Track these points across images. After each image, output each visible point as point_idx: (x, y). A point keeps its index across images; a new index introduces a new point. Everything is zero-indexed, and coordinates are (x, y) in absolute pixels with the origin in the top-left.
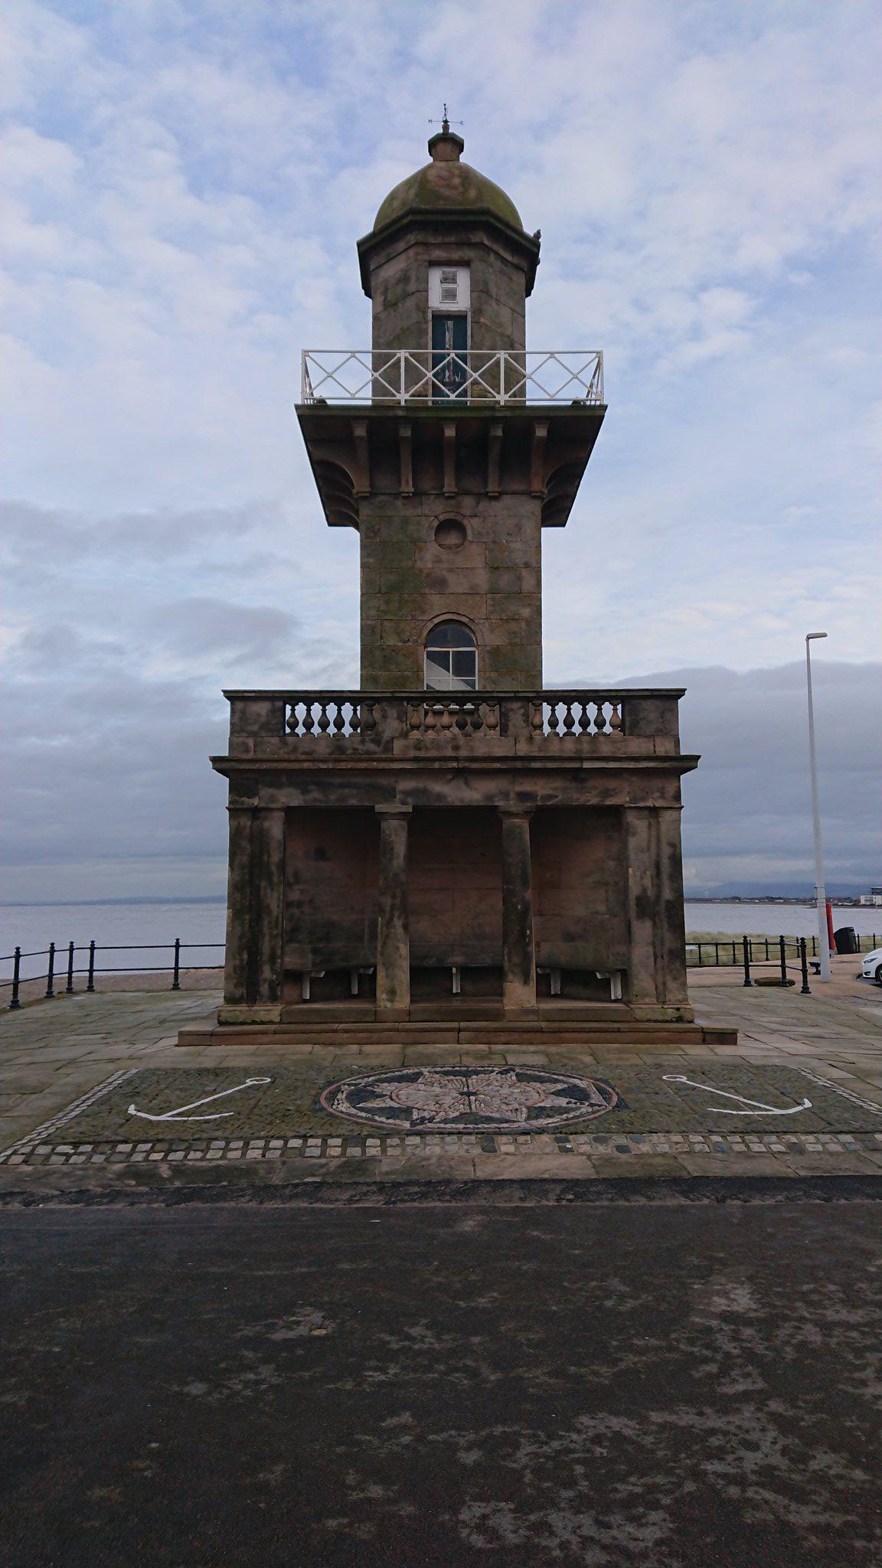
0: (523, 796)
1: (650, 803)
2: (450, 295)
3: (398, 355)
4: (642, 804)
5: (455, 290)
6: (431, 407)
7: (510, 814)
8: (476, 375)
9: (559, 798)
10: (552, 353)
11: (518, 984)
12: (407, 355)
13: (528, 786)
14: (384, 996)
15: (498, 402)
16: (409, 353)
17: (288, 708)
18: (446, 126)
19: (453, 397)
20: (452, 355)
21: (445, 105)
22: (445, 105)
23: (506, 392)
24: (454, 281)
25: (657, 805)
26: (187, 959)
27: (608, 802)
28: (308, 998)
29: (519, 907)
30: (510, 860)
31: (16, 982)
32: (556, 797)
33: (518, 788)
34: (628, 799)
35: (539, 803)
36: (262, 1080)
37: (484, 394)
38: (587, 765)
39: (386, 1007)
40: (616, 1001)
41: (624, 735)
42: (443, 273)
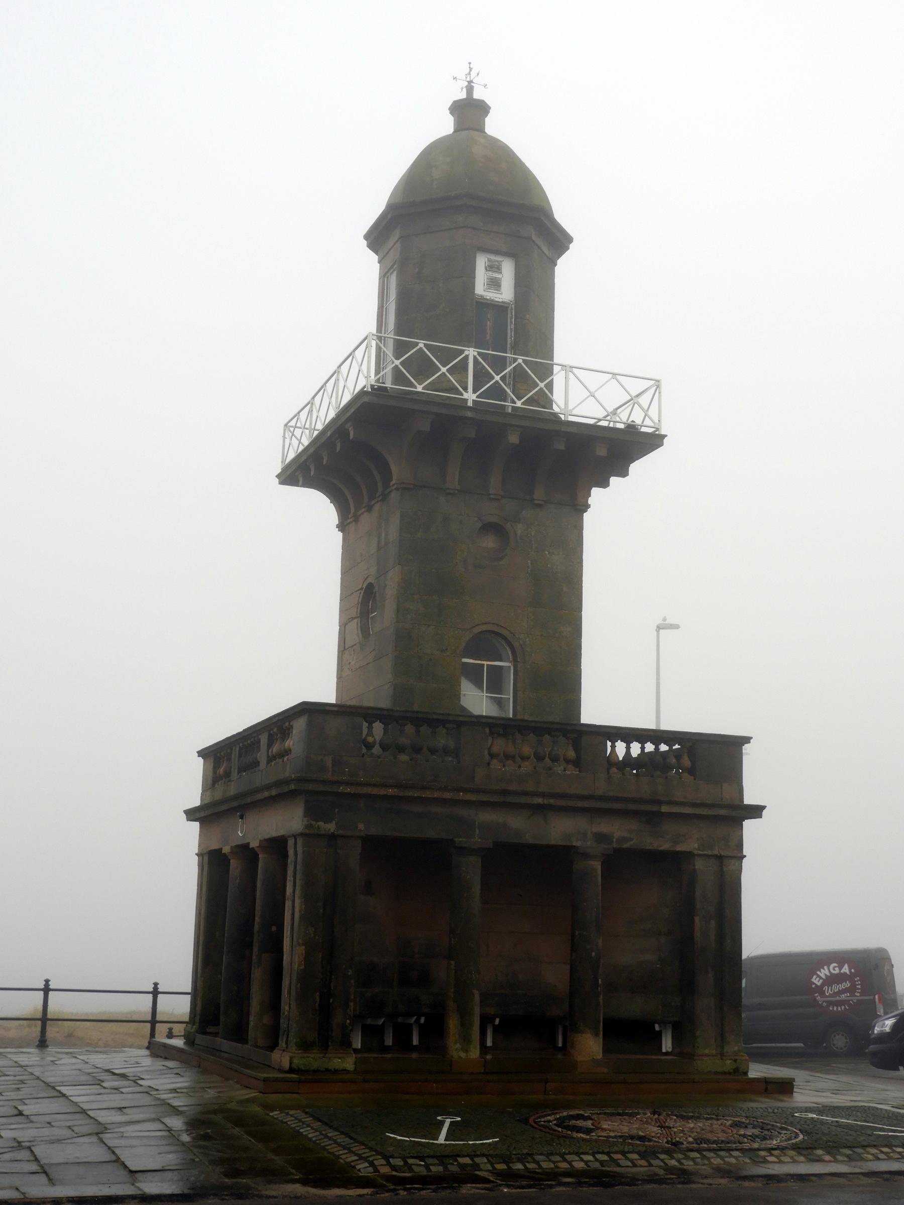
0: (601, 838)
1: (716, 852)
2: (495, 284)
3: (466, 353)
4: (709, 853)
5: (500, 279)
6: (510, 414)
7: (586, 856)
8: (397, 362)
9: (633, 841)
10: (614, 374)
11: (589, 1035)
12: (476, 354)
13: (605, 827)
14: (458, 1046)
15: (466, 400)
16: (424, 344)
17: (609, 744)
18: (470, 89)
19: (420, 388)
20: (421, 345)
21: (470, 63)
22: (470, 63)
23: (474, 391)
24: (498, 269)
25: (723, 854)
26: (59, 1004)
27: (678, 849)
28: (391, 1044)
29: (593, 954)
30: (585, 904)
31: (154, 1022)
32: (632, 840)
33: (596, 829)
34: (696, 845)
35: (615, 846)
36: (808, 1115)
37: (454, 390)
38: (665, 809)
39: (460, 1057)
40: (667, 1054)
41: (695, 779)
42: (489, 260)
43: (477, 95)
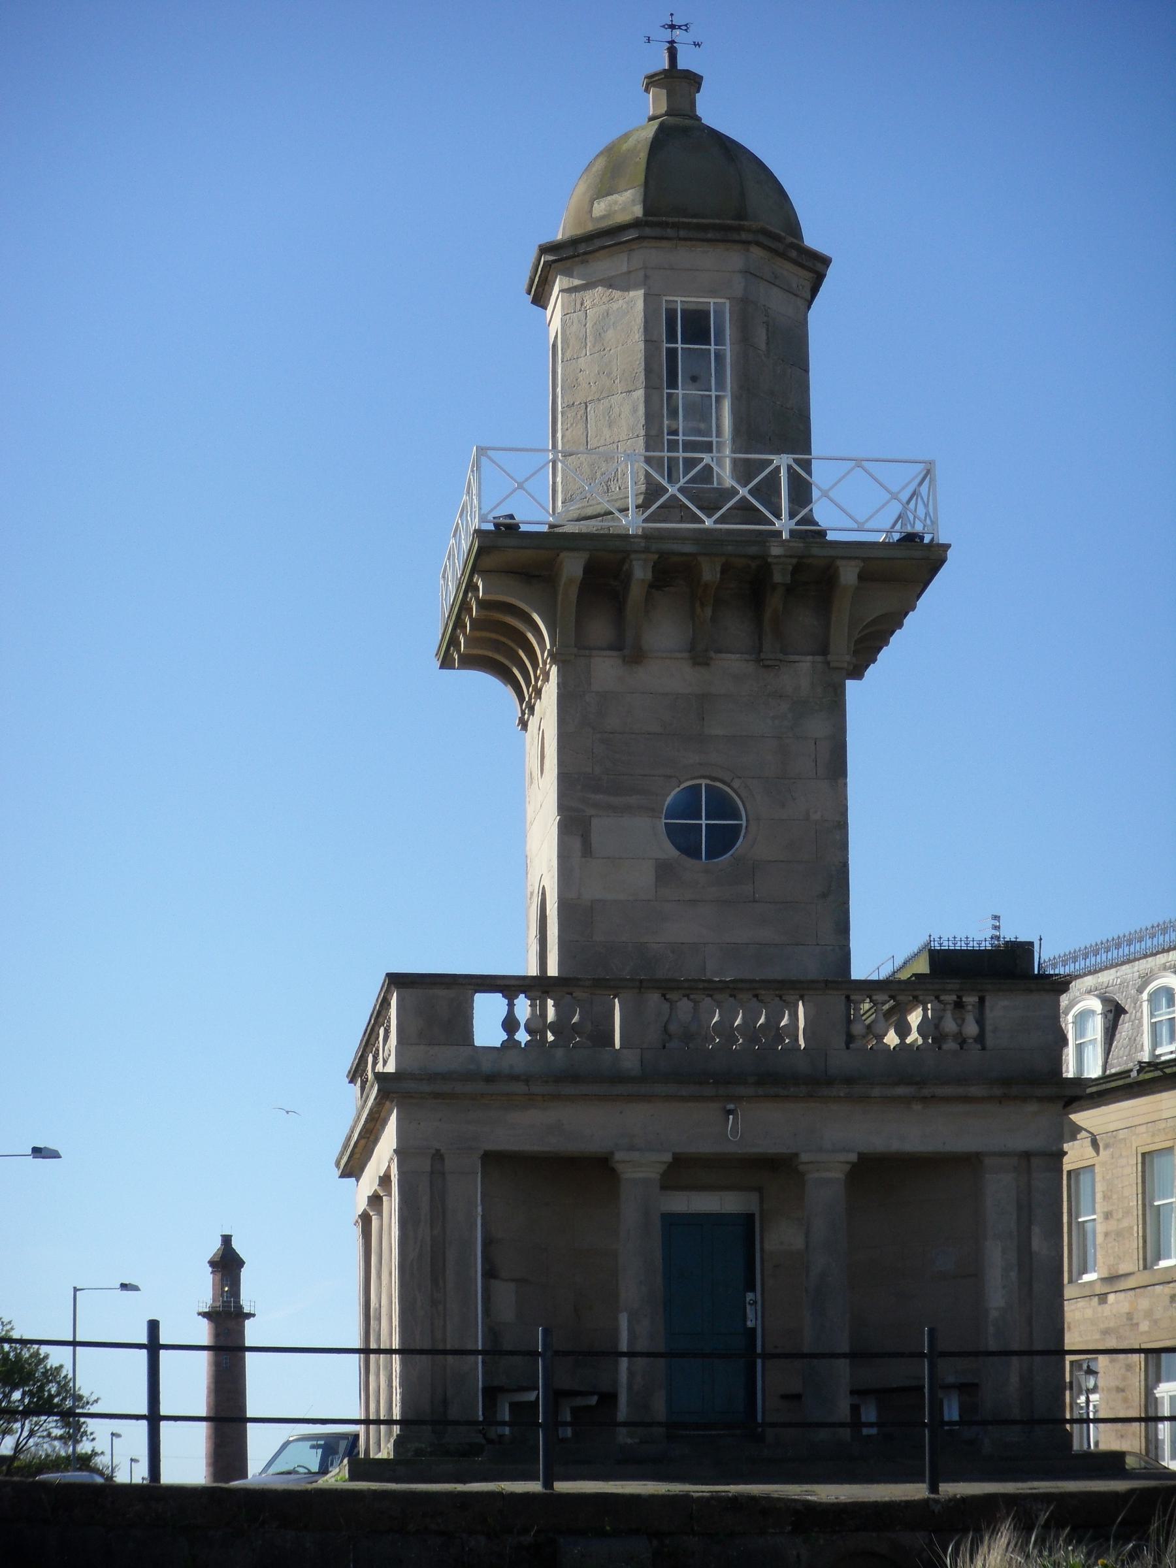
10: (859, 462)
12: (791, 462)
19: (708, 523)
43: (681, 65)
